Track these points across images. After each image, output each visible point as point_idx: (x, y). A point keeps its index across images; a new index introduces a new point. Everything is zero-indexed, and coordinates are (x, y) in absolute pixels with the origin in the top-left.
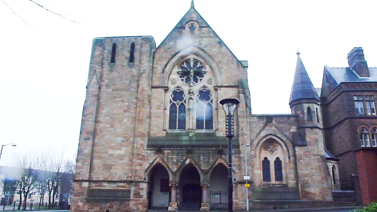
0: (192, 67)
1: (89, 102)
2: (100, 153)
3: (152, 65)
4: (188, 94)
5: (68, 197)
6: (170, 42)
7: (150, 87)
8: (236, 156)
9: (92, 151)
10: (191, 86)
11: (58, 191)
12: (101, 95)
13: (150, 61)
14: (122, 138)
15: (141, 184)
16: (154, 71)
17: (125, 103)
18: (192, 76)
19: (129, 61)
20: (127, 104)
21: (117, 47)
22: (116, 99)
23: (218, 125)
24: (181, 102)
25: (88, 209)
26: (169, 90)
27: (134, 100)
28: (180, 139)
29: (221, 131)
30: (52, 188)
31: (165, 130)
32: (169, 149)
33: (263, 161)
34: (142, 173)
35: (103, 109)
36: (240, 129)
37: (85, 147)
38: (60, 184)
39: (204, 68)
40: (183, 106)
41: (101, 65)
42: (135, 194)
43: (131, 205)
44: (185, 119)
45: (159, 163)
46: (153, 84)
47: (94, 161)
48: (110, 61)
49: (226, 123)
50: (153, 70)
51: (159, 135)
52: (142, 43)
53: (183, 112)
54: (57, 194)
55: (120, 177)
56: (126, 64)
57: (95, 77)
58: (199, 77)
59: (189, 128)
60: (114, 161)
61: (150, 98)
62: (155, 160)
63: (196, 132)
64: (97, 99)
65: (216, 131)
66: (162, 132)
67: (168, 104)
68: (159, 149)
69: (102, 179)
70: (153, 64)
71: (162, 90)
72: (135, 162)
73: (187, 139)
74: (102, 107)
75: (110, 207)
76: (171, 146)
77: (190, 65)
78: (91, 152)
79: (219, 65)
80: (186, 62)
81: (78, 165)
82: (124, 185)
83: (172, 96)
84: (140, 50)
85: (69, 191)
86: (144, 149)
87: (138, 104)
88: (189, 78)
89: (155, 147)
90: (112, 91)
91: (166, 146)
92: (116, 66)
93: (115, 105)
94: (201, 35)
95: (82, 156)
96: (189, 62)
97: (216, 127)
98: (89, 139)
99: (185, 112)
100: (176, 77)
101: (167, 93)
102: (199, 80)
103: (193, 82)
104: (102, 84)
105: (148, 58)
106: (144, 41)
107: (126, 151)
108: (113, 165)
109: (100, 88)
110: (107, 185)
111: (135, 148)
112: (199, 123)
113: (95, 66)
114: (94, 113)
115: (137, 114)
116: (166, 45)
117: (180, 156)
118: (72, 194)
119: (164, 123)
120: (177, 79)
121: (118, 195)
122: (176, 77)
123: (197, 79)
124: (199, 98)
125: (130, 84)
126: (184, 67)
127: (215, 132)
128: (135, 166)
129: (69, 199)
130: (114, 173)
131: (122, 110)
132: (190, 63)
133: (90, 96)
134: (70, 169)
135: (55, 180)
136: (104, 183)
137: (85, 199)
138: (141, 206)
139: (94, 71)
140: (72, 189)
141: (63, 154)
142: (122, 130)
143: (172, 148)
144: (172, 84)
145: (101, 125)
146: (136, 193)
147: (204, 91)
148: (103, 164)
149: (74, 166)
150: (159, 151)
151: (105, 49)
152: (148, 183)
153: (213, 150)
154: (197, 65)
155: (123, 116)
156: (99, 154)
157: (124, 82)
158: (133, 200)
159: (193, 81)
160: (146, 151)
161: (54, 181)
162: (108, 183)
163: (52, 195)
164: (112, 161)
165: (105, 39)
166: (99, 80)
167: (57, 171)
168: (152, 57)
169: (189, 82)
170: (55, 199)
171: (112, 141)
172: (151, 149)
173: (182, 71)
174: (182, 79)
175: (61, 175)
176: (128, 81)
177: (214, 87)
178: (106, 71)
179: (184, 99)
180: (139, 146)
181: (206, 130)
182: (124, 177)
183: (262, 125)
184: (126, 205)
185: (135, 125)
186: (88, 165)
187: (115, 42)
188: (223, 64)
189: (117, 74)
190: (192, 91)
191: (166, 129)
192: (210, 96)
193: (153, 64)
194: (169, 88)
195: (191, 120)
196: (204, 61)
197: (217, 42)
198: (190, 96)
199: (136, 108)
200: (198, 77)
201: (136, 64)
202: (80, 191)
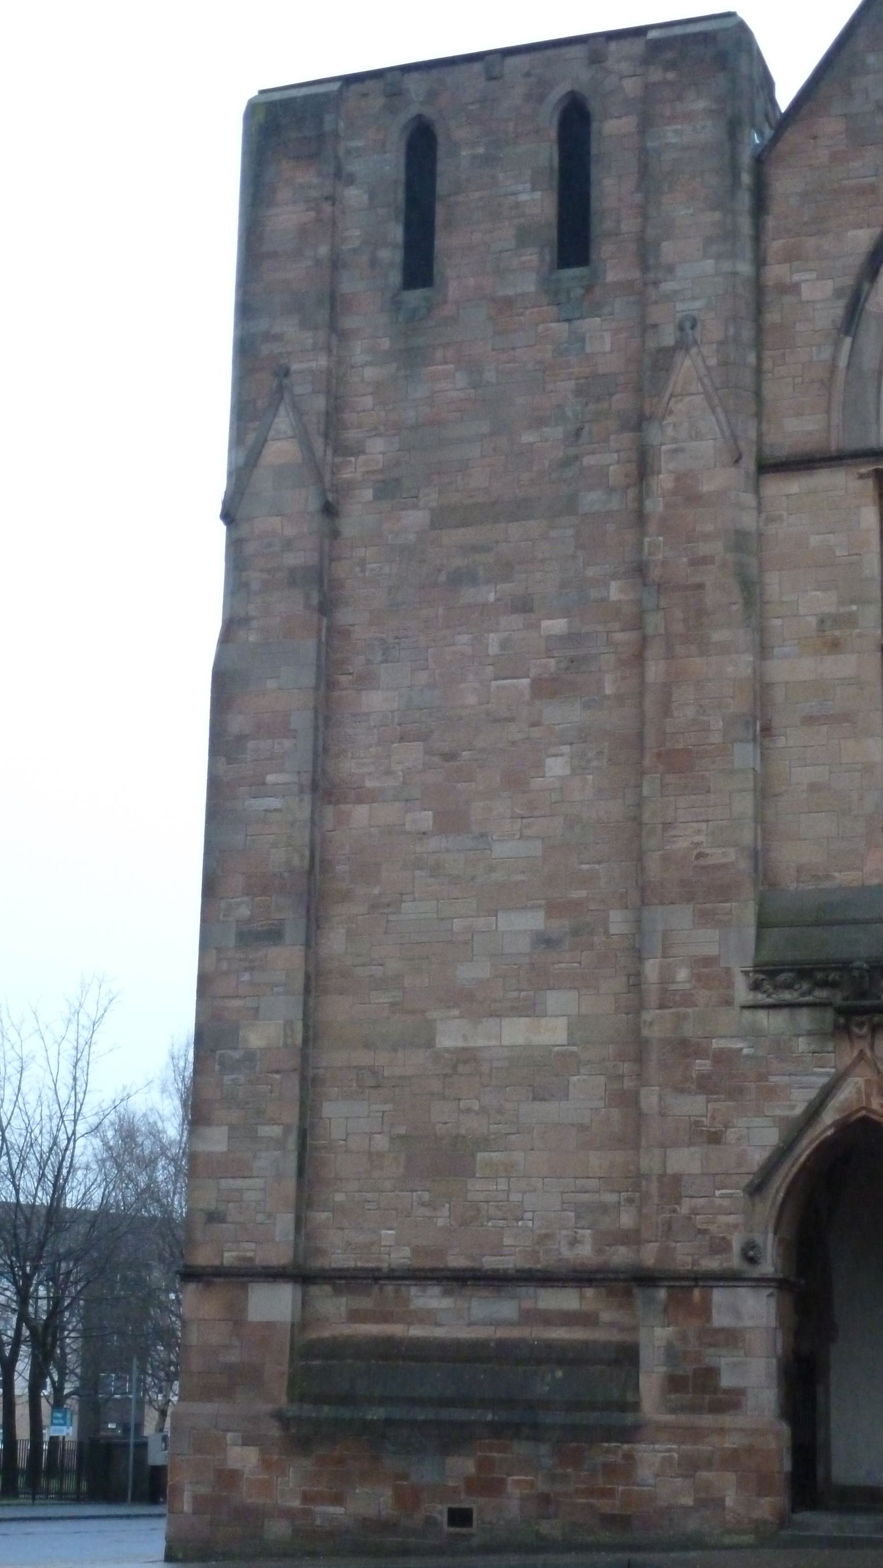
1: (252, 638)
2: (367, 1045)
3: (745, 268)
5: (140, 1403)
7: (749, 464)
9: (306, 1026)
11: (64, 1355)
12: (341, 570)
13: (730, 235)
14: (541, 915)
15: (719, 1296)
16: (772, 317)
17: (545, 623)
19: (550, 255)
20: (557, 626)
21: (442, 150)
22: (468, 595)
25: (307, 1498)
27: (615, 591)
30: (18, 1331)
34: (726, 1203)
35: (366, 681)
37: (250, 1003)
38: (75, 1299)
41: (322, 316)
43: (645, 1472)
45: (865, 1120)
46: (768, 439)
47: (328, 1109)
48: (395, 278)
50: (759, 309)
51: (843, 878)
52: (647, 87)
54: (62, 1380)
55: (546, 1236)
56: (528, 284)
57: (283, 422)
60: (483, 1110)
61: (754, 562)
62: (827, 1093)
64: (315, 599)
68: (863, 995)
70: (760, 262)
71: (855, 484)
72: (663, 1115)
74: (358, 663)
75: (474, 1486)
78: (299, 1040)
81: (201, 1147)
82: (588, 1307)
84: (643, 151)
85: (144, 1355)
86: (728, 1002)
87: (654, 622)
89: (824, 984)
90: (433, 526)
92: (448, 310)
95: (227, 1079)
98: (274, 935)
104: (346, 475)
105: (717, 216)
106: (672, 65)
107: (577, 1022)
108: (484, 1143)
109: (329, 510)
110: (447, 1303)
111: (653, 996)
113: (276, 329)
114: (302, 720)
115: (650, 705)
118: (170, 1378)
121: (542, 1389)
125: (572, 451)
128: (663, 1146)
129: (151, 1418)
130: (492, 1211)
131: (524, 683)
133: (255, 586)
134: (142, 1180)
135: (36, 1269)
136: (413, 1290)
137: (279, 1416)
138: (731, 1477)
139: (276, 374)
140: (165, 1335)
141: (82, 1064)
142: (536, 848)
143: (809, 992)
145: (360, 813)
146: (687, 1369)
148: (401, 1137)
149: (174, 1160)
150: (865, 1011)
151: (351, 180)
152: (782, 1284)
155: (536, 732)
156: (362, 1058)
157: (527, 438)
158: (661, 1427)
160: (747, 1013)
161: (28, 1278)
162: (446, 1293)
163: (21, 1386)
164: (468, 1110)
165: (340, 91)
166: (319, 444)
167: (44, 1199)
168: (745, 200)
170: (46, 1419)
172: (787, 996)
175: (82, 1229)
176: (556, 432)
178: (365, 365)
180: (683, 974)
182: (574, 1242)
184: (610, 1470)
185: (639, 805)
186: (280, 1144)
187: (429, 112)
189: (461, 379)
193: (760, 262)
199: (639, 658)
201: (611, 277)
202: (233, 1357)
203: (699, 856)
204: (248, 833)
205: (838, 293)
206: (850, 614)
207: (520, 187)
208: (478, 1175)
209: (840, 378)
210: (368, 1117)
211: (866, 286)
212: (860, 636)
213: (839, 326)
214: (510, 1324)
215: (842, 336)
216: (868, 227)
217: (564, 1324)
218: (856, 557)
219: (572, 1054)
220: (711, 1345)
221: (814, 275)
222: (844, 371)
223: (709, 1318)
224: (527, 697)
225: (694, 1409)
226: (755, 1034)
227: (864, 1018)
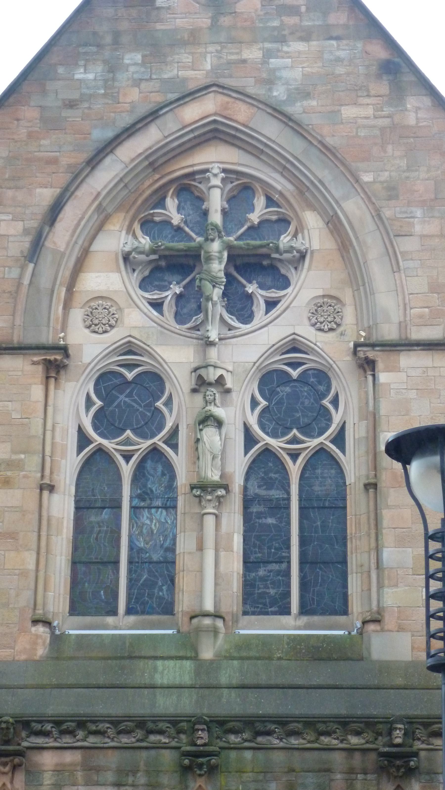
0: (216, 227)
4: (194, 391)
6: (76, 65)
10: (211, 344)
18: (215, 283)
23: (380, 586)
24: (150, 442)
26: (72, 363)
28: (138, 681)
29: (401, 629)
31: (47, 623)
32: (67, 740)
39: (292, 229)
40: (160, 468)
44: (172, 549)
49: (429, 577)
53: (158, 503)
58: (262, 286)
59: (197, 610)
63: (242, 632)
65: (371, 627)
66: (23, 630)
67: (64, 455)
71: (29, 368)
73: (187, 680)
76: (81, 724)
77: (206, 213)
79: (387, 213)
80: (178, 194)
83: (89, 403)
88: (200, 292)
91: (48, 727)
94: (276, 23)
96: (201, 191)
97: (370, 604)
101: (57, 387)
102: (263, 306)
103: (222, 319)
112: (261, 572)
116: (50, 86)
119: (41, 574)
120: (122, 301)
123: (250, 297)
124: (96, 416)
126: (167, 223)
127: (361, 633)
132: (201, 199)
147: (295, 374)
153: (350, 751)
154: (252, 209)
159: (220, 310)
169: (201, 316)
173: (153, 251)
174: (155, 295)
179: (169, 424)
181: (305, 619)
188: (409, 204)
190: (219, 372)
191: (50, 617)
192: (331, 407)
194: (70, 352)
195: (210, 555)
196: (290, 187)
197: (374, 69)
198: (207, 403)
200: (251, 288)
205: (26, 232)
206: (21, 460)
209: (24, 290)
211: (47, 229)
212: (25, 477)
213: (25, 254)
215: (27, 262)
216: (51, 187)
218: (27, 420)
221: (10, 217)
222: (27, 286)
227: (7, 759)
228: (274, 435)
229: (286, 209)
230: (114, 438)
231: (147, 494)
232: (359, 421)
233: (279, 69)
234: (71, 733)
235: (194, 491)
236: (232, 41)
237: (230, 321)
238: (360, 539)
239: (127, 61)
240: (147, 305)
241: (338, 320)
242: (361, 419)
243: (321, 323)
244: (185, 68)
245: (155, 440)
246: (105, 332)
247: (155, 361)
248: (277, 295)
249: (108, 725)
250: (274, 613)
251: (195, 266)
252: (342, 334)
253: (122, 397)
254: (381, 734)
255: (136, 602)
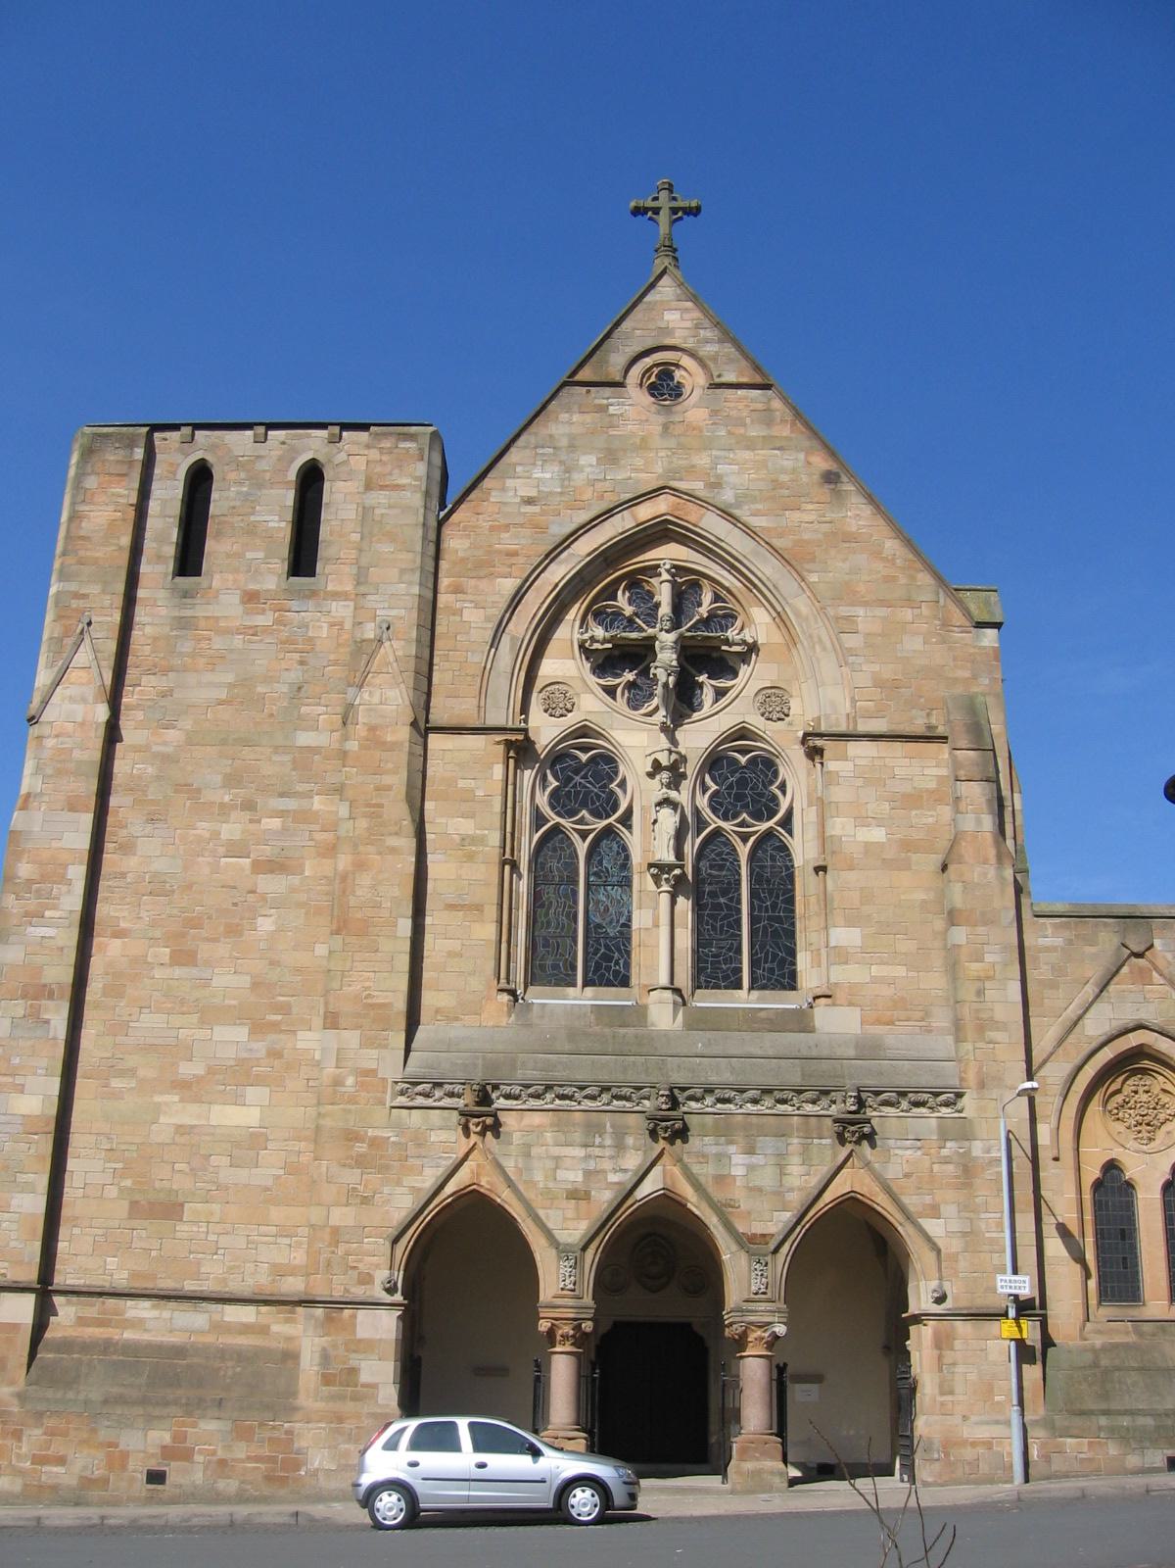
8: (945, 1152)
32: (533, 1103)
33: (1098, 1185)
36: (968, 992)
39: (738, 624)
42: (327, 1379)
44: (627, 925)
63: (699, 1005)
69: (121, 1280)
75: (168, 1453)
80: (627, 588)
82: (263, 1320)
89: (451, 1095)
93: (203, 828)
99: (630, 886)
100: (574, 672)
110: (155, 1313)
117: (608, 1152)
120: (577, 685)
122: (574, 672)
126: (618, 614)
132: (651, 595)
142: (245, 981)
144: (546, 711)
154: (700, 605)
155: (251, 898)
171: (187, 1052)
174: (610, 681)
177: (806, 735)
183: (1095, 972)
192: (778, 793)
197: (816, 477)
203: (368, 996)
204: (439, 714)
206: (486, 836)
207: (272, 518)
208: (185, 1220)
210: (103, 1172)
214: (202, 1332)
217: (241, 1333)
219: (262, 1134)
220: (355, 1351)
223: (354, 1332)
224: (248, 872)
225: (341, 1398)
226: (400, 1128)
228: (725, 818)
229: (733, 604)
230: (570, 817)
231: (603, 872)
232: (808, 806)
233: (727, 475)
234: (537, 1096)
235: (652, 870)
236: (681, 446)
237: (650, 708)
238: (809, 920)
239: (582, 462)
240: (602, 692)
241: (786, 711)
242: (810, 805)
243: (770, 713)
244: (636, 470)
245: (611, 820)
246: (562, 716)
247: (578, 745)
248: (614, 683)
249: (575, 1089)
250: (726, 988)
251: (646, 656)
252: (790, 724)
253: (577, 779)
254: (834, 1102)
255: (594, 973)
